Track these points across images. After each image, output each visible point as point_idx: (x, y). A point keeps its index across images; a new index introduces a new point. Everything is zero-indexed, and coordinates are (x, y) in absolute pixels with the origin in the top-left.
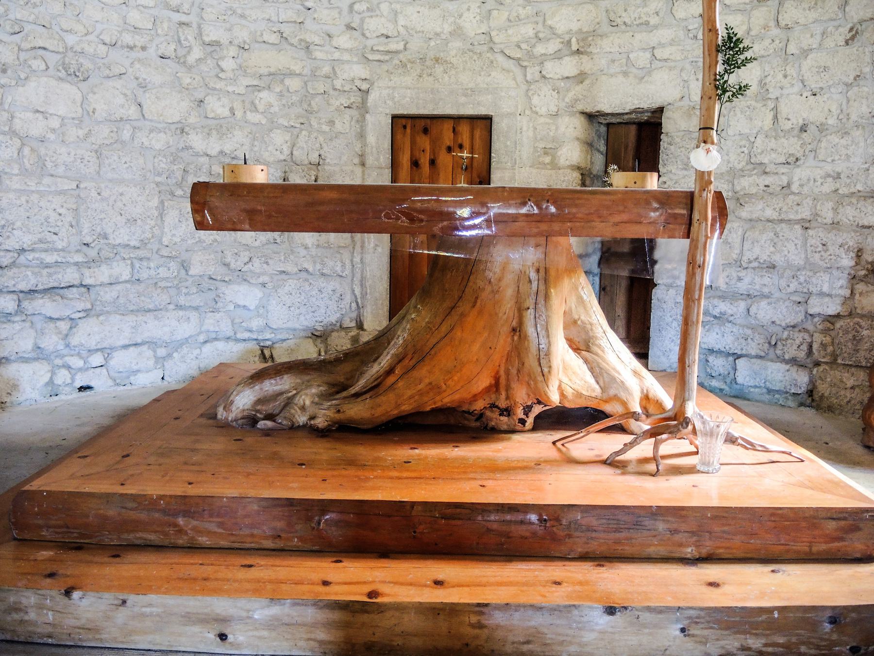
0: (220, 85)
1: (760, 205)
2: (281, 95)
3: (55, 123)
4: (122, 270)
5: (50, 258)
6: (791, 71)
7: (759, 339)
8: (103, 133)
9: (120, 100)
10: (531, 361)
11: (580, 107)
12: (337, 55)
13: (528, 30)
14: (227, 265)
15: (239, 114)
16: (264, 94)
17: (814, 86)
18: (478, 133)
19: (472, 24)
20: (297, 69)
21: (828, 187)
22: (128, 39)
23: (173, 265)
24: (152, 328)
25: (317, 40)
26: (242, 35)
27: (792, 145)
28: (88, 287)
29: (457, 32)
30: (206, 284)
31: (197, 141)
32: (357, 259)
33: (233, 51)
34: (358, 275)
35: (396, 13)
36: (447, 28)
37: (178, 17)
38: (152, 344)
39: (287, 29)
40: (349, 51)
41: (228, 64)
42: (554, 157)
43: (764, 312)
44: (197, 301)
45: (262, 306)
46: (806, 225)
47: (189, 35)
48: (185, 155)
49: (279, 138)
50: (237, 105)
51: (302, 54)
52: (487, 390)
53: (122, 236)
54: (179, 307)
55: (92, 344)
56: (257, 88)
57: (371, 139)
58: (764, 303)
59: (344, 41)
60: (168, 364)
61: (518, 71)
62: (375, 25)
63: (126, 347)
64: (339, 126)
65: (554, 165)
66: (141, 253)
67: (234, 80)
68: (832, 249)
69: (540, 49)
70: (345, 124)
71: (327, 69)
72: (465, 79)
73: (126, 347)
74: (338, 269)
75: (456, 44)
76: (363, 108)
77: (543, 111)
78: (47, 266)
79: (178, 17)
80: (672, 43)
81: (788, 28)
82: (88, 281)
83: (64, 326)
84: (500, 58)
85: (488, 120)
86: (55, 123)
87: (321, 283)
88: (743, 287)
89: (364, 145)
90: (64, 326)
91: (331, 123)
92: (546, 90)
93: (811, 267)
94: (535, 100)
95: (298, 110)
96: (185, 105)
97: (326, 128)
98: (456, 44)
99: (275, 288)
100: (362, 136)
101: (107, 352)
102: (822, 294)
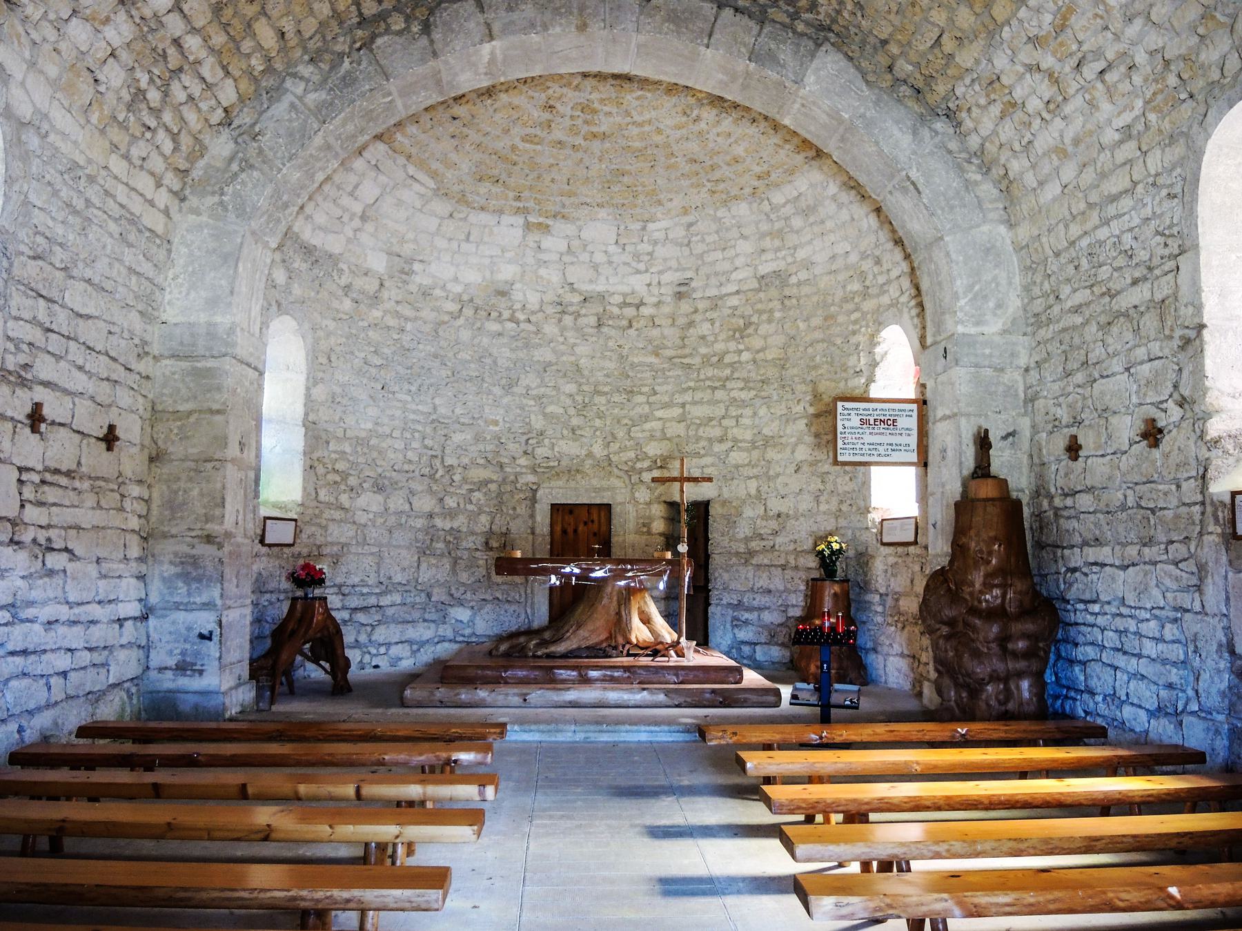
0: (452, 490)
1: (761, 556)
2: (485, 494)
3: (371, 516)
4: (397, 598)
5: (365, 590)
6: (771, 485)
7: (766, 633)
8: (392, 520)
9: (401, 501)
10: (624, 625)
11: (663, 498)
12: (518, 469)
13: (632, 455)
14: (452, 595)
15: (462, 506)
16: (476, 494)
17: (782, 493)
18: (602, 514)
19: (598, 450)
20: (495, 478)
21: (792, 547)
22: (406, 467)
23: (423, 595)
24: (412, 633)
25: (506, 461)
26: (466, 461)
27: (773, 524)
28: (380, 607)
29: (590, 455)
30: (440, 606)
31: (438, 522)
32: (529, 591)
33: (460, 470)
34: (128, 747)
35: (553, 445)
36: (584, 452)
37: (431, 453)
38: (410, 642)
39: (490, 457)
40: (526, 467)
41: (457, 478)
42: (649, 528)
43: (768, 617)
44: (434, 617)
45: (472, 621)
46: (784, 567)
47: (437, 462)
48: (431, 530)
49: (484, 519)
50: (462, 502)
51: (498, 469)
52: (607, 639)
53: (399, 578)
54: (425, 621)
55: (381, 640)
56: (471, 491)
57: (538, 518)
58: (766, 612)
59: (523, 461)
60: (418, 655)
61: (626, 478)
62: (541, 452)
63: (397, 643)
64: (518, 510)
65: (649, 533)
66: (407, 588)
67: (460, 487)
68: (796, 580)
69: (639, 465)
70: (522, 510)
71: (512, 478)
72: (595, 482)
73: (397, 643)
74: (517, 597)
75: (589, 462)
76: (534, 500)
77: (642, 501)
78: (363, 595)
79: (431, 453)
80: (713, 465)
81: (768, 461)
82: (381, 604)
83: (369, 629)
84: (615, 470)
85: (609, 506)
86: (371, 516)
87: (507, 606)
88: (755, 603)
89: (534, 522)
90: (369, 629)
91: (514, 509)
92: (643, 488)
93: (786, 590)
94: (637, 495)
95: (495, 502)
96: (434, 502)
97: (511, 512)
98: (589, 462)
99: (480, 610)
100: (532, 516)
101: (388, 645)
102: (793, 606)
